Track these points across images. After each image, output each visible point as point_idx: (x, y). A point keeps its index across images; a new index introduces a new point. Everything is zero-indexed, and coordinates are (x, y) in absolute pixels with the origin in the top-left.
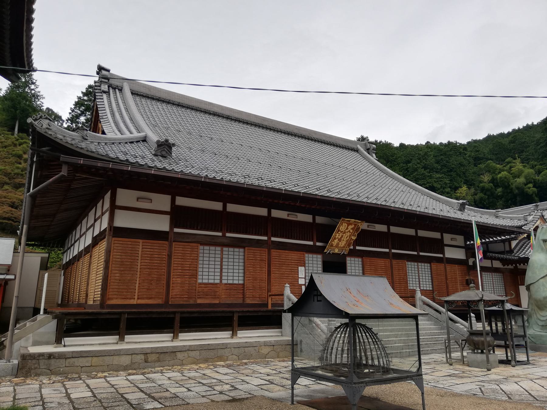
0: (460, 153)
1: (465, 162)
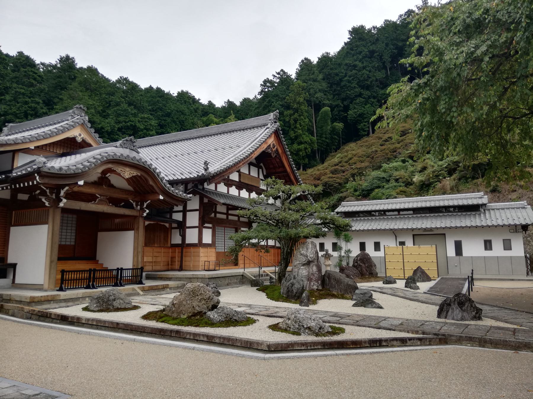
0: (185, 102)
1: (187, 111)
